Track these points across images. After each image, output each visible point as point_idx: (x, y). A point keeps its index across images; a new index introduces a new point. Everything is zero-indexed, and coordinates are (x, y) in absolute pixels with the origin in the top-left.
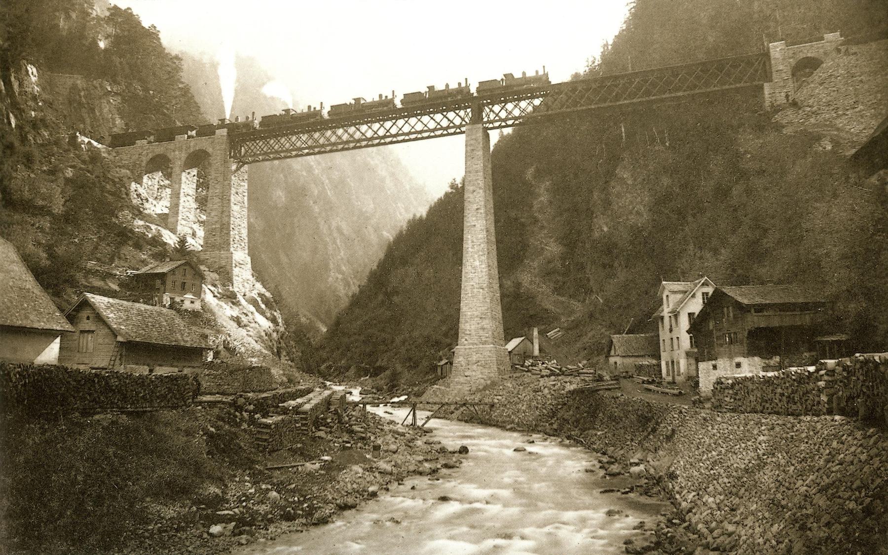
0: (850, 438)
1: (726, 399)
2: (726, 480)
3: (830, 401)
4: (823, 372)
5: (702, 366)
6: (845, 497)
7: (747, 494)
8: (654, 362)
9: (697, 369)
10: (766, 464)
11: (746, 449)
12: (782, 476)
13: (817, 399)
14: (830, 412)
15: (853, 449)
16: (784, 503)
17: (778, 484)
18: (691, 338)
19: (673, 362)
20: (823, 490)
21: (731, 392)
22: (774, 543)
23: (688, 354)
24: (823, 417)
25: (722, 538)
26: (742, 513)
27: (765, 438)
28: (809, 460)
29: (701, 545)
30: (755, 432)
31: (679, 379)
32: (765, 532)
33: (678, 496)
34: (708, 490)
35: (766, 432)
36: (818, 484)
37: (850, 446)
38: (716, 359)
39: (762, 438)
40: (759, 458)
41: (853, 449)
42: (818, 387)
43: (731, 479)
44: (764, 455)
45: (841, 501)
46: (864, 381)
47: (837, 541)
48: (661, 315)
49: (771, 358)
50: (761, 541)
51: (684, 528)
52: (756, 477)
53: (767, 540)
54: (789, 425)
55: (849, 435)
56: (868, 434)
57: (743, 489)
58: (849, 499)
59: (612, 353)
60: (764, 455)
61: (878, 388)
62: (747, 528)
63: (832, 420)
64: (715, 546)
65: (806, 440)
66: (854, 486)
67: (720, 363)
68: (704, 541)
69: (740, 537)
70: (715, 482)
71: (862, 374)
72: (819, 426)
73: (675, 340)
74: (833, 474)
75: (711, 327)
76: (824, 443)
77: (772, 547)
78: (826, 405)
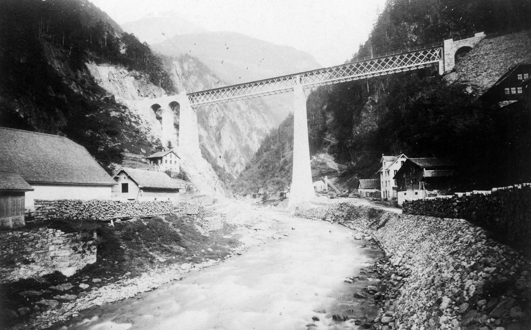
0: (467, 231)
1: (409, 208)
2: (407, 245)
3: (459, 212)
4: (456, 198)
5: (399, 193)
6: (462, 259)
7: (416, 251)
8: (378, 190)
9: (397, 195)
10: (426, 238)
11: (417, 231)
12: (433, 244)
13: (452, 211)
14: (459, 217)
15: (468, 236)
16: (433, 257)
17: (431, 248)
18: (395, 181)
19: (386, 191)
20: (452, 254)
21: (411, 205)
22: (427, 277)
23: (394, 188)
24: (455, 219)
25: (404, 271)
26: (413, 260)
27: (426, 227)
28: (446, 239)
29: (395, 273)
30: (422, 224)
31: (389, 199)
32: (423, 270)
33: (385, 250)
34: (399, 248)
35: (427, 224)
36: (450, 251)
37: (467, 234)
38: (406, 190)
39: (425, 227)
40: (423, 236)
41: (468, 236)
42: (453, 205)
43: (410, 244)
44: (425, 234)
45: (460, 261)
46: (477, 204)
47: (456, 280)
48: (382, 171)
49: (433, 191)
50: (421, 274)
51: (388, 265)
52: (421, 244)
53: (424, 274)
54: (438, 222)
55: (466, 229)
56: (476, 230)
57: (415, 249)
58: (464, 260)
59: (360, 187)
60: (425, 234)
61: (484, 208)
62: (415, 267)
63: (459, 221)
64: (400, 274)
65: (446, 229)
66: (467, 254)
67: (407, 192)
68: (396, 271)
69: (412, 271)
70: (402, 245)
71: (476, 200)
72: (452, 223)
73: (388, 182)
74: (457, 247)
75: (404, 177)
76: (454, 232)
77: (425, 278)
78: (457, 214)
